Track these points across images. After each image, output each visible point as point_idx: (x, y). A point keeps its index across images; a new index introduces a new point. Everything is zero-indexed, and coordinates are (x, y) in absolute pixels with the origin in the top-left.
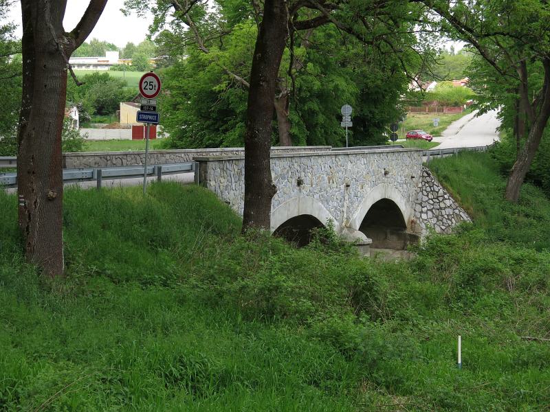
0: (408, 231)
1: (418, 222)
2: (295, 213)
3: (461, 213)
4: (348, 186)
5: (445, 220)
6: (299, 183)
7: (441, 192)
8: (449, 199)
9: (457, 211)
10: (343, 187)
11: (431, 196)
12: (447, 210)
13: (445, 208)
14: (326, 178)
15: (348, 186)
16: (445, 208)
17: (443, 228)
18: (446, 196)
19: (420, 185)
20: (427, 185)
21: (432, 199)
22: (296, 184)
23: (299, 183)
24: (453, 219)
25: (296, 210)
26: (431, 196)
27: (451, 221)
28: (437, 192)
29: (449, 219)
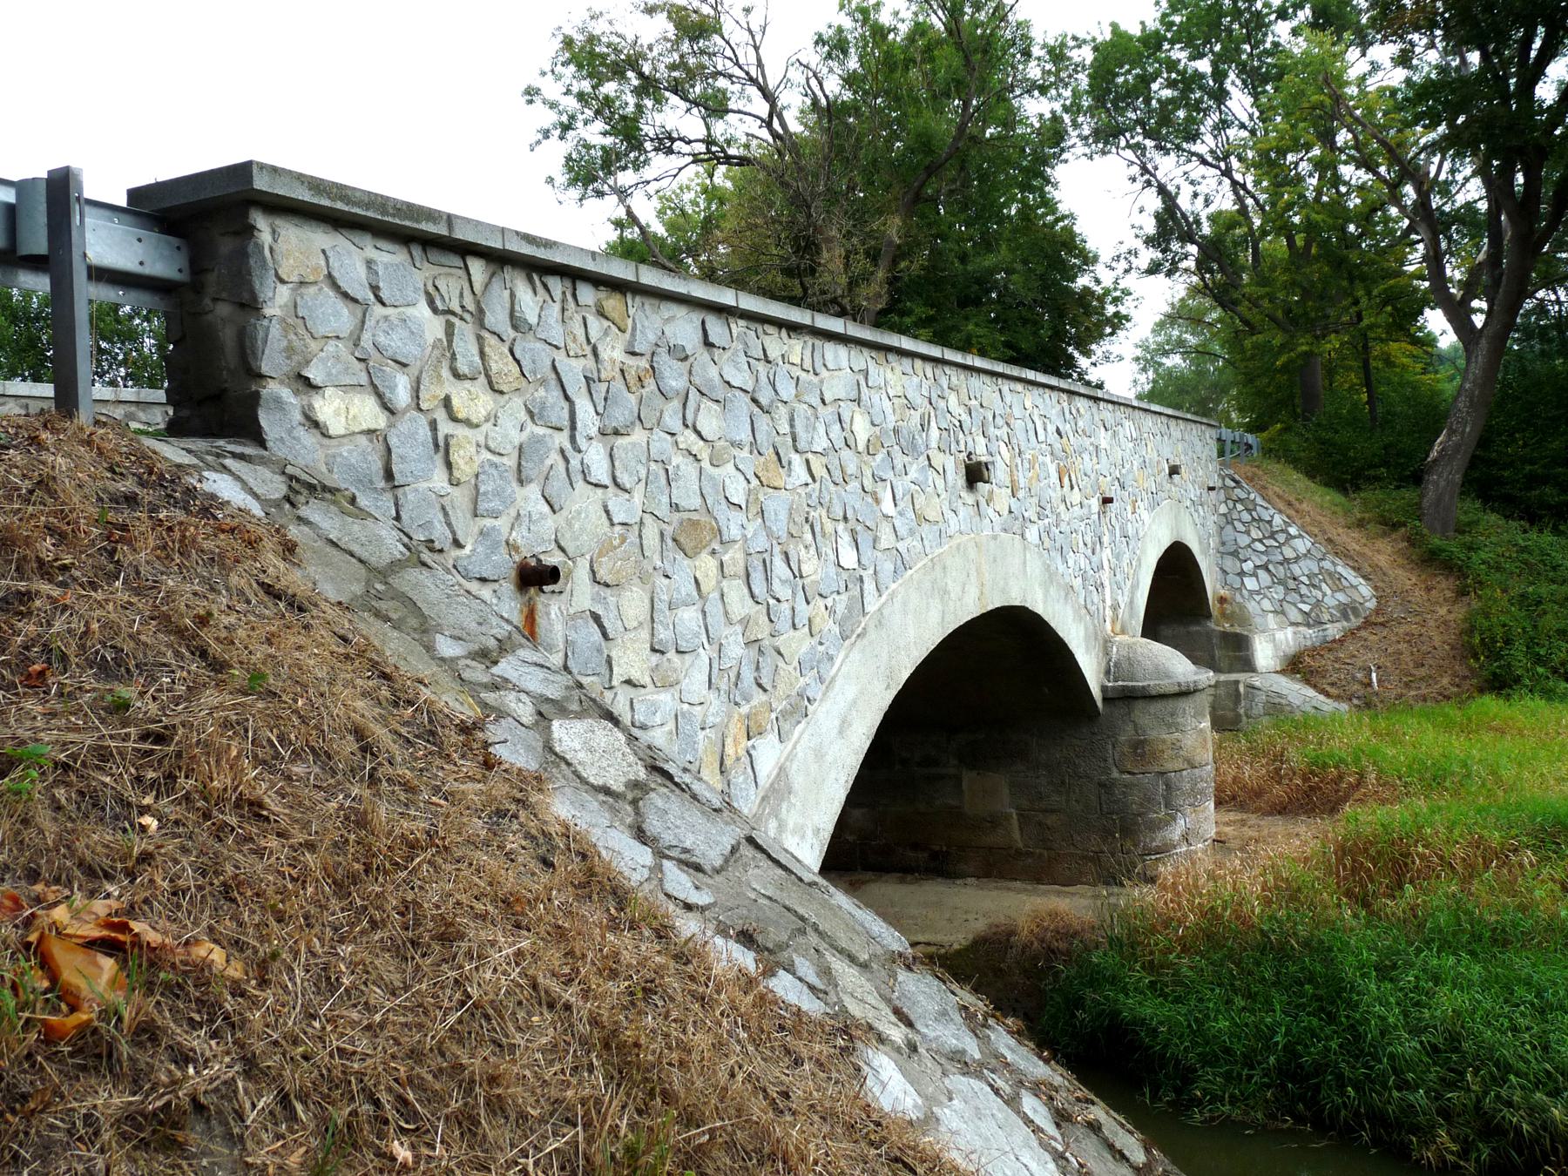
0: (1217, 625)
1: (1238, 598)
2: (969, 609)
3: (1340, 569)
4: (1107, 501)
5: (1304, 590)
6: (975, 474)
7: (1278, 520)
8: (1300, 536)
9: (1327, 564)
10: (1095, 504)
11: (1255, 534)
12: (1302, 563)
13: (1297, 559)
14: (1052, 469)
15: (1107, 501)
16: (1297, 559)
17: (1306, 608)
18: (1293, 531)
19: (1223, 509)
20: (1240, 507)
21: (1260, 541)
22: (961, 481)
23: (975, 474)
24: (1324, 586)
25: (973, 592)
26: (1255, 534)
27: (1320, 589)
28: (1270, 522)
29: (1314, 586)
